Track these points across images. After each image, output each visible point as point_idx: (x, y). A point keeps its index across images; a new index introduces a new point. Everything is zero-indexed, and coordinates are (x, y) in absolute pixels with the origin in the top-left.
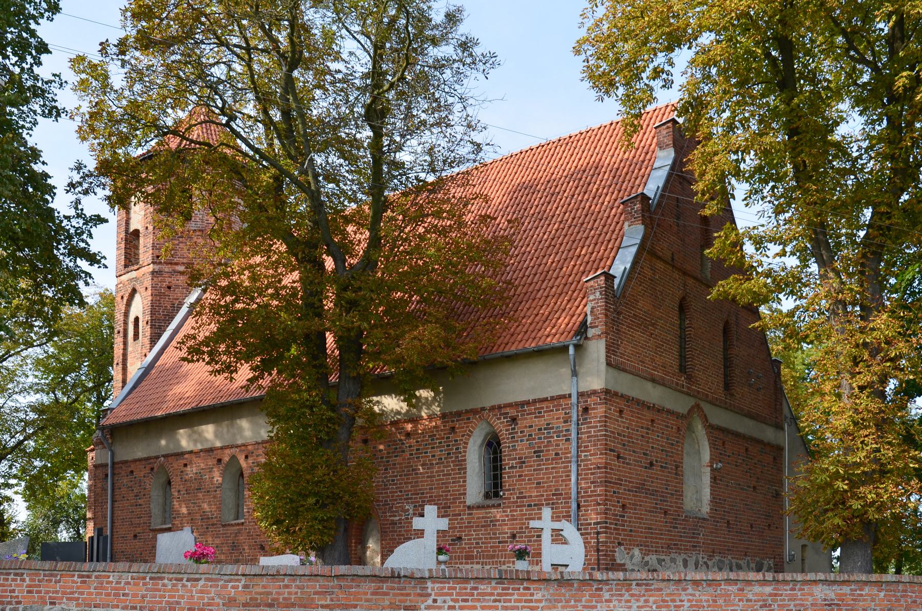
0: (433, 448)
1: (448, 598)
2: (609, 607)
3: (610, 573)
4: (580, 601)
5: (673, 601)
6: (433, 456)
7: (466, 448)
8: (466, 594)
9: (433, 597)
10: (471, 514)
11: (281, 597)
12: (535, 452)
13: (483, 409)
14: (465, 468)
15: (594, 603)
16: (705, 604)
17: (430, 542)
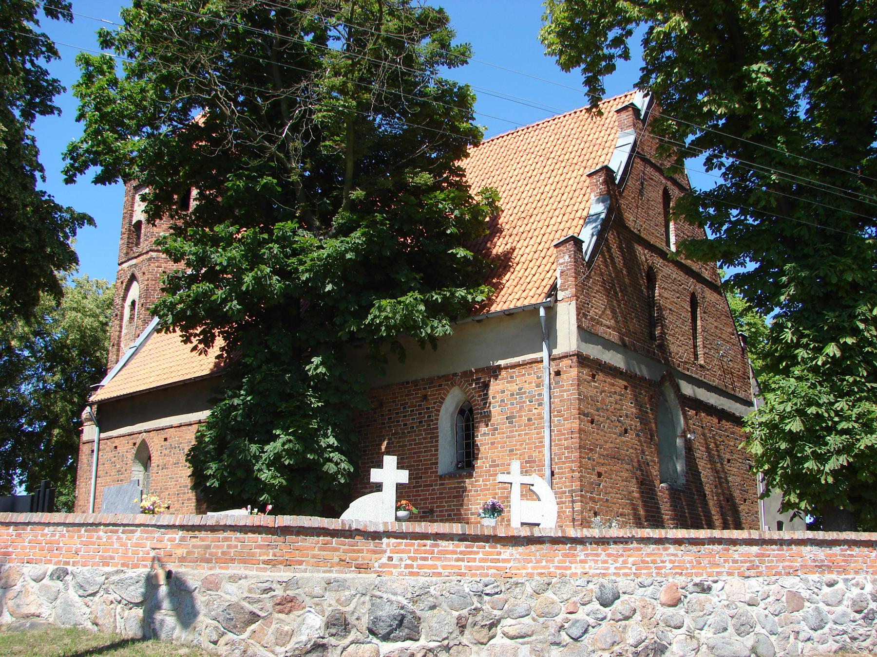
0: (405, 416)
1: (405, 556)
2: (584, 568)
3: (585, 530)
4: (552, 561)
5: (654, 562)
6: (405, 425)
7: (438, 415)
8: (426, 552)
9: (388, 554)
10: (443, 484)
11: (220, 551)
12: (507, 418)
13: (455, 375)
14: (437, 437)
15: (567, 564)
16: (688, 565)
17: (389, 494)
